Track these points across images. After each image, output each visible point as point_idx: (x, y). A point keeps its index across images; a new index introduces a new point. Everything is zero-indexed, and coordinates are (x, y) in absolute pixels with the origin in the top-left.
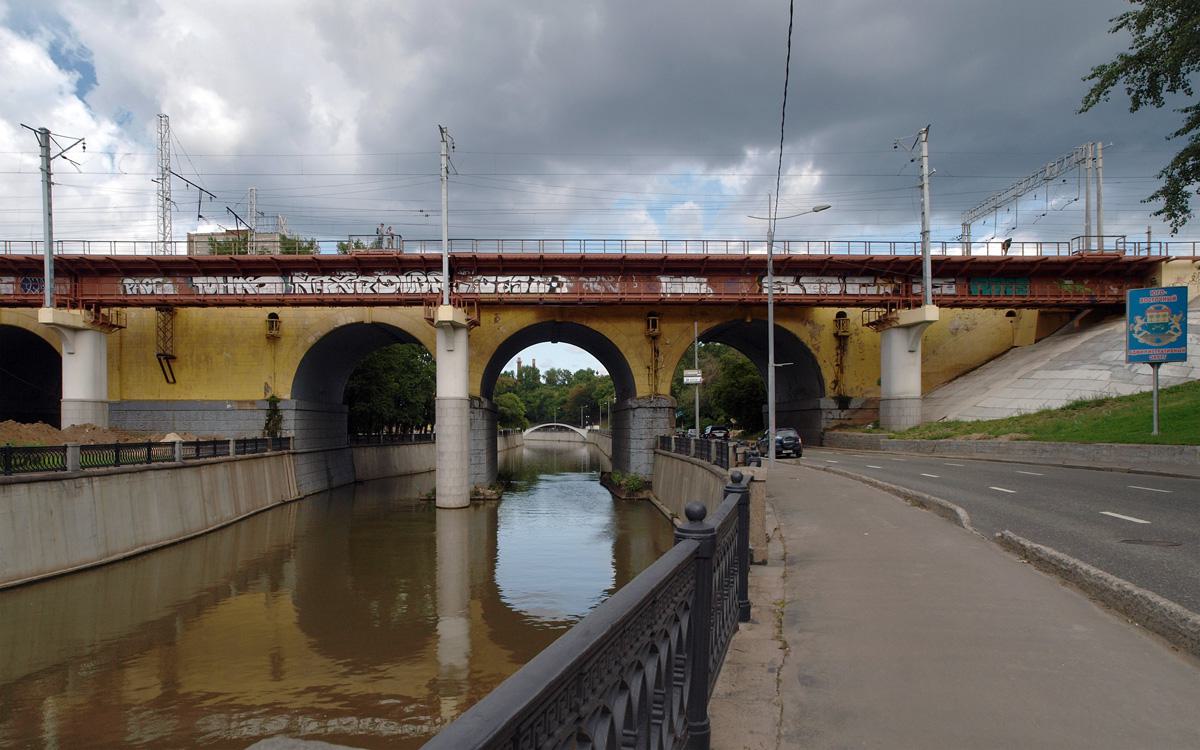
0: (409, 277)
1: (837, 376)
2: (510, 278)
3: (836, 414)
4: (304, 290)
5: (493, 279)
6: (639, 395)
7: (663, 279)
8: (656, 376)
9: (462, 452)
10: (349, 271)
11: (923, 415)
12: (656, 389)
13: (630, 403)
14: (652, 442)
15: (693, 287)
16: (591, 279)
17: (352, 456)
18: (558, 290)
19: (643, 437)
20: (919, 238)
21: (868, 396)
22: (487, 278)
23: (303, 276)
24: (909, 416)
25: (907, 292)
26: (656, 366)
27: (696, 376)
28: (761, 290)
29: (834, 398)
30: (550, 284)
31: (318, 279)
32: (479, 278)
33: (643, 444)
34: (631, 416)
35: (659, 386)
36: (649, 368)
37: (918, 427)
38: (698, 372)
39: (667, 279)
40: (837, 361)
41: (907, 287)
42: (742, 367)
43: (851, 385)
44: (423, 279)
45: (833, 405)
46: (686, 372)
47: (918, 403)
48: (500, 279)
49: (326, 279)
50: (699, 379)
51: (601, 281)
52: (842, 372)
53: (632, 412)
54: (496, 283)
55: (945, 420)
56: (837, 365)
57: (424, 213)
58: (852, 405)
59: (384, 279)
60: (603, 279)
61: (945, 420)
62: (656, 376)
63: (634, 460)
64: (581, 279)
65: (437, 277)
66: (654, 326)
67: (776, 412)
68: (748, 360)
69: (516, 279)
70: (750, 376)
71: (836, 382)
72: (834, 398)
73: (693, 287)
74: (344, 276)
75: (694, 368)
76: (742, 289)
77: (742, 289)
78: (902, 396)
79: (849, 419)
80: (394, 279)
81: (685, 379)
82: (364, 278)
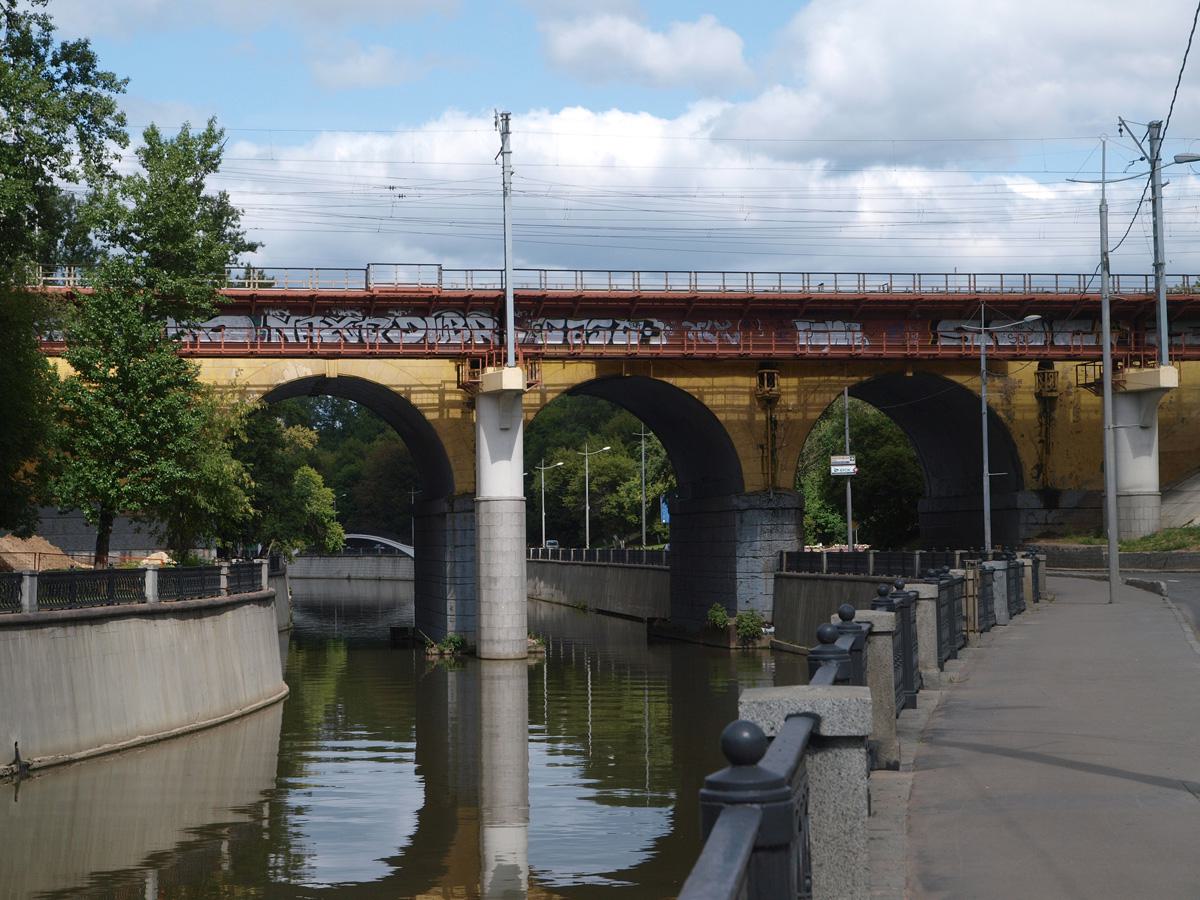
0: (439, 320)
1: (1040, 459)
2: (584, 322)
3: (1041, 515)
4: (286, 338)
5: (560, 324)
6: (748, 489)
7: (801, 326)
8: (773, 460)
9: (521, 577)
10: (351, 309)
11: (1161, 519)
12: (773, 477)
13: (735, 501)
14: (773, 561)
15: (836, 338)
16: (700, 325)
17: (923, 513)
18: (654, 341)
19: (759, 553)
20: (1151, 270)
21: (1088, 488)
22: (553, 322)
23: (283, 315)
24: (1148, 518)
25: (1136, 343)
26: (773, 444)
27: (847, 464)
28: (934, 342)
29: (1037, 492)
30: (642, 332)
31: (304, 321)
32: (540, 321)
33: (759, 565)
34: (738, 522)
35: (778, 475)
36: (762, 447)
37: (1154, 535)
38: (850, 459)
39: (806, 325)
40: (1040, 435)
41: (1136, 336)
42: (874, 430)
43: (1061, 469)
44: (460, 323)
45: (1035, 502)
46: (835, 459)
47: (1155, 501)
48: (572, 324)
49: (316, 321)
50: (851, 469)
51: (713, 326)
52: (1048, 452)
53: (738, 517)
54: (565, 330)
55: (1191, 525)
56: (1041, 441)
57: (397, 192)
58: (1064, 502)
59: (403, 322)
60: (716, 324)
61: (1191, 525)
62: (773, 460)
63: (742, 590)
64: (685, 324)
65: (481, 320)
66: (771, 383)
67: (983, 511)
68: (886, 418)
69: (594, 323)
70: (889, 447)
71: (1040, 468)
72: (1037, 492)
73: (836, 338)
74: (343, 318)
75: (844, 454)
76: (914, 344)
77: (914, 344)
78: (1132, 491)
79: (1061, 524)
80: (418, 322)
81: (833, 469)
82: (374, 321)
